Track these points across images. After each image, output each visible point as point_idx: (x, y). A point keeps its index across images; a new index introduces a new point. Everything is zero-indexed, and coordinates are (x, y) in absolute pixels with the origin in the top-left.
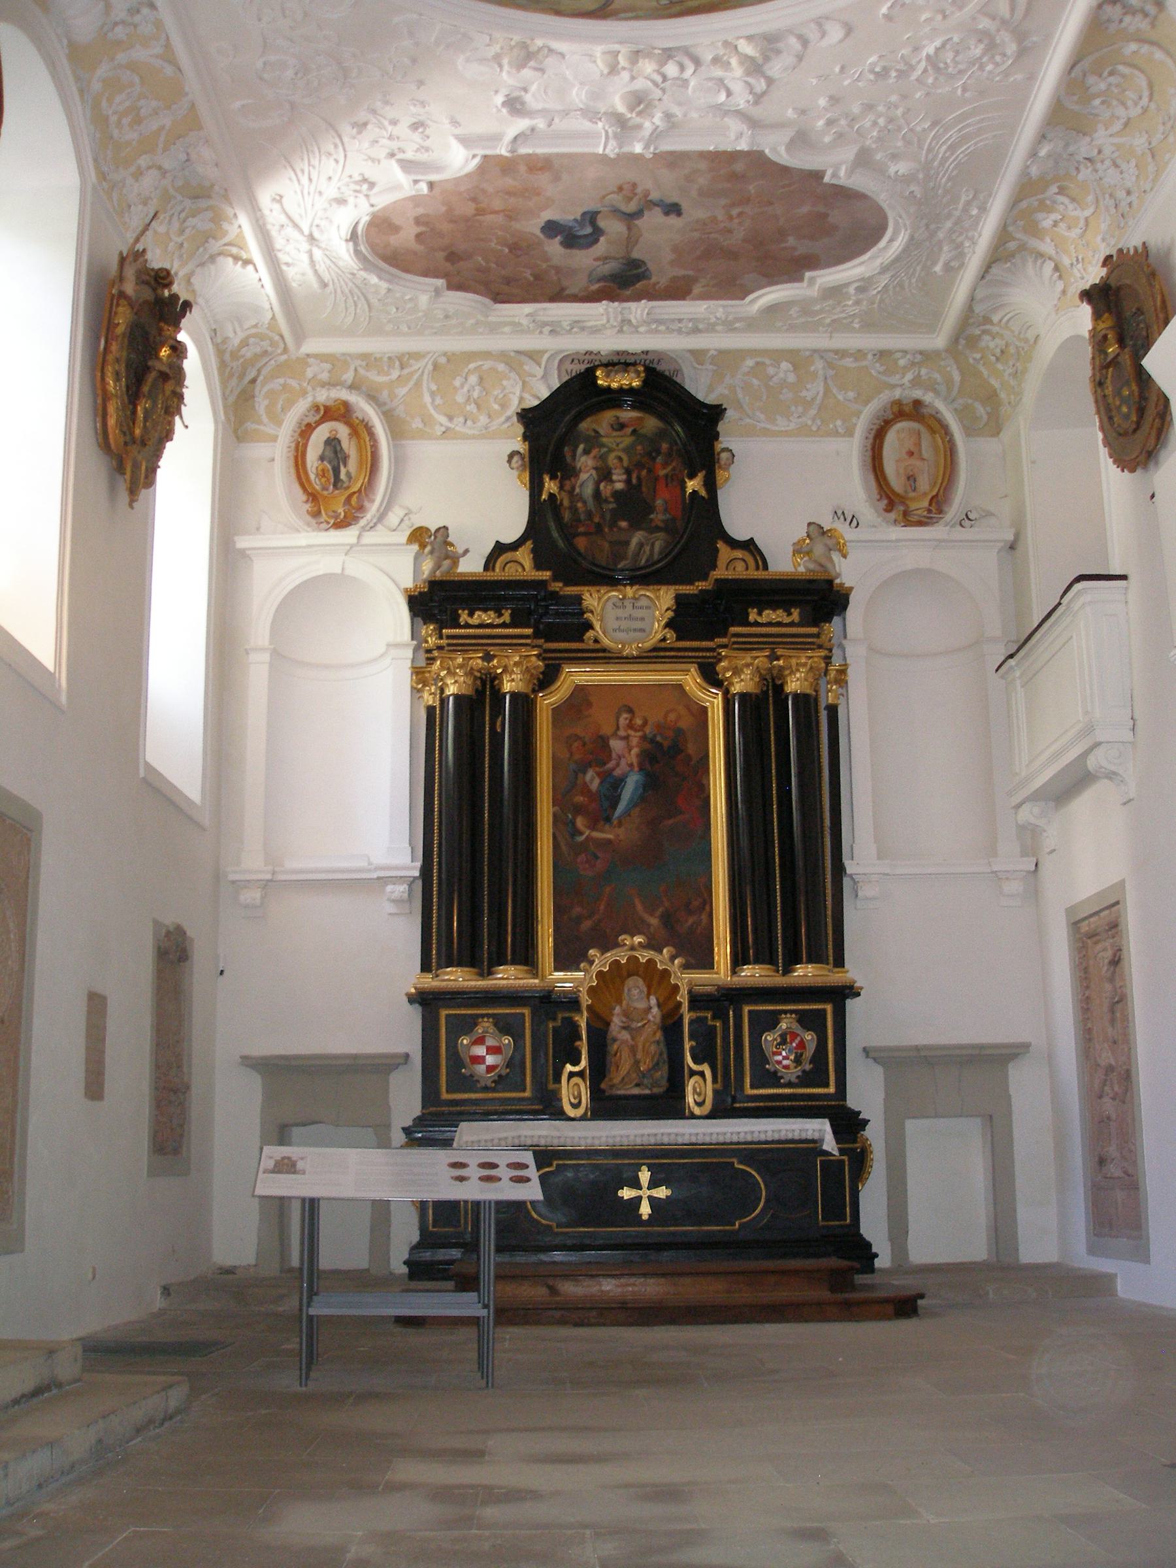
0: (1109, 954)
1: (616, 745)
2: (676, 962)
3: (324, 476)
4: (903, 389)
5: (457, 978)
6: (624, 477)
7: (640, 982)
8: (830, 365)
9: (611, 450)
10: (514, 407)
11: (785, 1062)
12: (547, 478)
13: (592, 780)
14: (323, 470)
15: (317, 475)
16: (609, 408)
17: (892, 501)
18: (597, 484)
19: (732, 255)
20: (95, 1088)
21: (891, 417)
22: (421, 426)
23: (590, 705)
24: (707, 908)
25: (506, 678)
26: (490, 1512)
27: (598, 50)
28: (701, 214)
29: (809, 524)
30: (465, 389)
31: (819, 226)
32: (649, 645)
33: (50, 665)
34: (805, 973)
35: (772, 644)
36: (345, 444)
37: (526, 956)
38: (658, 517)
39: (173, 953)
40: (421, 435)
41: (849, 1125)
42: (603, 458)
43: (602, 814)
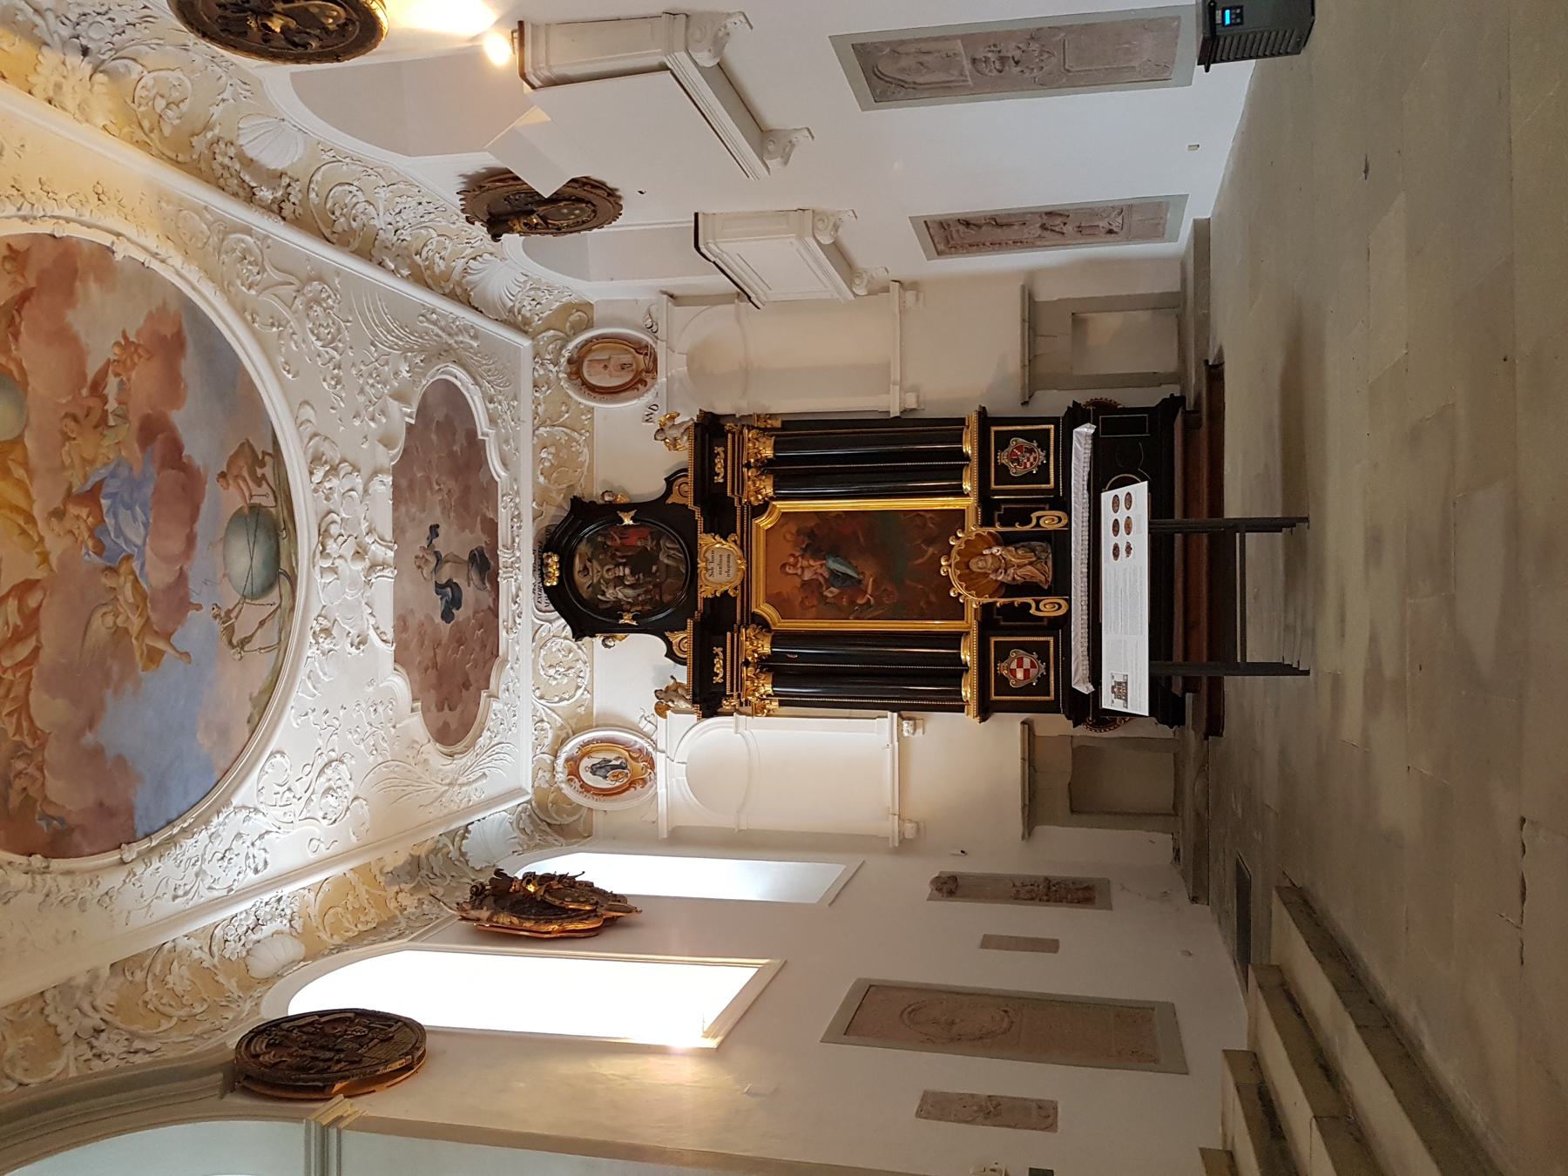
0: (961, 228)
4: (559, 372)
5: (968, 692)
7: (974, 561)
8: (543, 424)
10: (572, 644)
17: (638, 382)
19: (466, 490)
20: (1051, 946)
23: (779, 594)
24: (924, 47)
26: (1389, 672)
27: (319, 581)
28: (438, 510)
31: (446, 428)
32: (739, 552)
33: (752, 972)
35: (739, 465)
37: (954, 639)
38: (650, 545)
39: (949, 887)
40: (589, 712)
41: (1076, 415)
42: (607, 582)
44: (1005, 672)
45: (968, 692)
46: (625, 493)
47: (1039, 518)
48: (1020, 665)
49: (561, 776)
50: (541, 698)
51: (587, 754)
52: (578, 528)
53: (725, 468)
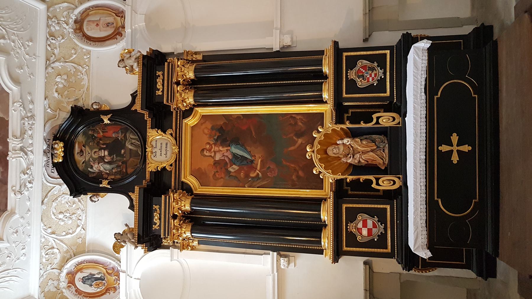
1: (218, 157)
2: (320, 130)
3: (98, 285)
4: (69, 29)
5: (327, 241)
6: (103, 151)
7: (330, 148)
9: (91, 157)
11: (373, 76)
12: (101, 186)
13: (234, 168)
14: (96, 285)
15: (98, 288)
16: (73, 155)
17: (117, 33)
18: (106, 163)
21: (81, 33)
22: (81, 240)
23: (200, 168)
24: (294, 116)
25: (183, 208)
29: (119, 66)
30: (64, 219)
32: (174, 141)
34: (327, 68)
35: (173, 83)
36: (86, 275)
37: (317, 203)
38: (120, 136)
40: (84, 240)
42: (94, 160)
43: (249, 164)
44: (354, 230)
45: (327, 241)
46: (109, 104)
47: (378, 118)
48: (365, 225)
49: (63, 284)
50: (53, 233)
51: (80, 270)
52: (78, 125)
53: (163, 85)
